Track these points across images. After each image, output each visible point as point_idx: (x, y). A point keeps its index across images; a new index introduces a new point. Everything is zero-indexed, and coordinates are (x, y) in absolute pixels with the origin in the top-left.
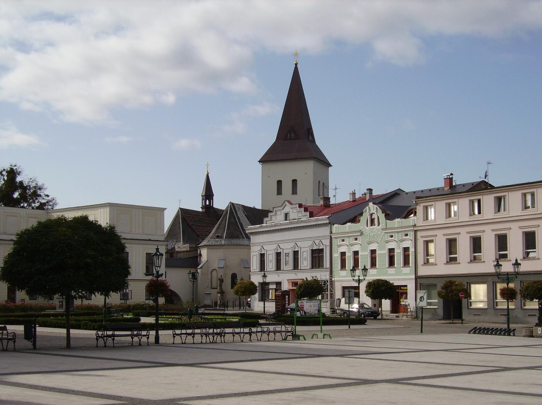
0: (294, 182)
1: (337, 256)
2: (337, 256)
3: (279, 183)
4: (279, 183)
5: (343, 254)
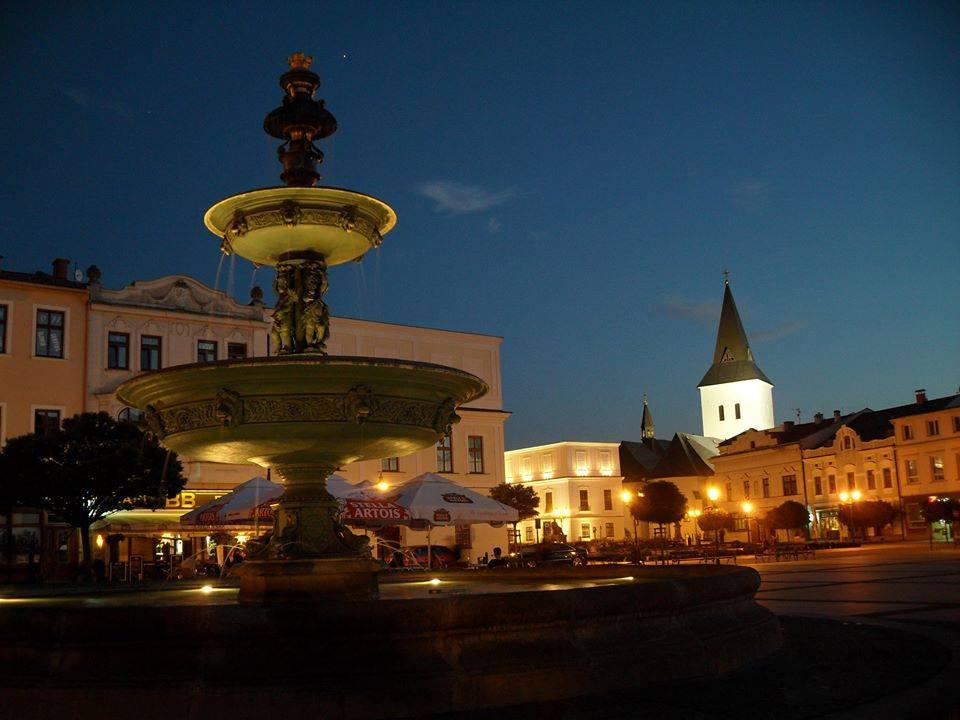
0: (737, 407)
1: (810, 481)
2: (810, 481)
3: (721, 409)
4: (721, 409)
5: (817, 480)
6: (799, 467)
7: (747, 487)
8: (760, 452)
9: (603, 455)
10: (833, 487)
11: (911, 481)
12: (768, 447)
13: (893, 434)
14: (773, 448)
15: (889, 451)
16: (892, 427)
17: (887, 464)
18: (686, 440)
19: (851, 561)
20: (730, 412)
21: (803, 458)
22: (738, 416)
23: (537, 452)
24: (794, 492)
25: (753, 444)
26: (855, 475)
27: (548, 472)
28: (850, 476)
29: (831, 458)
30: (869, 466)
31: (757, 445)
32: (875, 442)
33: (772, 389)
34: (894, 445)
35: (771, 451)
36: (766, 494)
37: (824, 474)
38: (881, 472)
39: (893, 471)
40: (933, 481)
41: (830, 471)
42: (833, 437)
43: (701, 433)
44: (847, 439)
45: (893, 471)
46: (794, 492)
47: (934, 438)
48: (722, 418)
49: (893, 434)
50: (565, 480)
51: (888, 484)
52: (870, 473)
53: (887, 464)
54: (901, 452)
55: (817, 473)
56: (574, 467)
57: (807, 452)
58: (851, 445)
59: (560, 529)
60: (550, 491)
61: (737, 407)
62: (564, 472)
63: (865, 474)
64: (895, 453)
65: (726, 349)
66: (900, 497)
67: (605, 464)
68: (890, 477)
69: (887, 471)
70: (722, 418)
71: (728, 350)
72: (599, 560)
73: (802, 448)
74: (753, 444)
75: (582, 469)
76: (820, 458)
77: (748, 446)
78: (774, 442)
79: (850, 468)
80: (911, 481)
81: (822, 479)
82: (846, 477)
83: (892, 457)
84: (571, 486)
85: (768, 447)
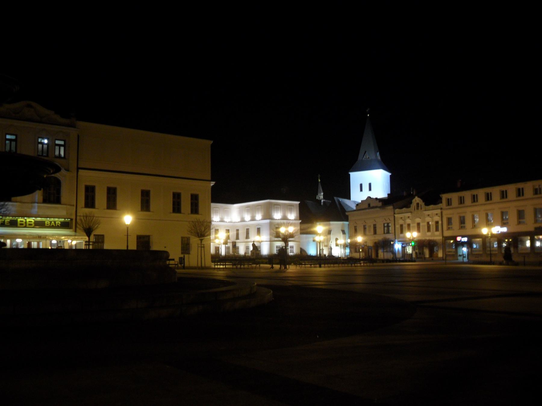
0: (370, 185)
1: (398, 226)
2: (398, 226)
4: (361, 185)
6: (392, 219)
7: (365, 228)
8: (372, 210)
9: (290, 208)
10: (402, 232)
11: (448, 229)
12: (376, 207)
13: (441, 202)
14: (380, 207)
15: (439, 211)
16: (441, 199)
17: (437, 218)
18: (339, 201)
19: (410, 267)
20: (366, 187)
21: (394, 214)
22: (370, 189)
23: (253, 205)
24: (388, 232)
25: (369, 205)
26: (421, 224)
27: (259, 216)
28: (418, 224)
29: (409, 214)
30: (428, 219)
31: (371, 205)
32: (432, 206)
33: (390, 176)
34: (441, 209)
35: (378, 209)
36: (375, 233)
37: (405, 223)
38: (434, 223)
39: (440, 222)
40: (460, 229)
41: (408, 221)
42: (411, 203)
43: (349, 197)
44: (418, 204)
45: (440, 222)
46: (388, 232)
47: (462, 205)
48: (361, 190)
49: (441, 202)
50: (268, 221)
51: (437, 230)
52: (428, 223)
53: (437, 218)
54: (445, 212)
55: (401, 222)
56: (273, 214)
57: (397, 210)
58: (420, 208)
59: (238, 248)
60: (248, 228)
61: (370, 185)
62: (268, 216)
63: (426, 224)
64: (442, 213)
65: (365, 152)
66: (443, 237)
67: (291, 213)
68: (438, 226)
69: (437, 223)
70: (361, 190)
71: (367, 153)
72: (220, 268)
73: (395, 208)
74: (369, 205)
75: (277, 215)
76: (403, 214)
77: (367, 206)
78: (380, 204)
79: (418, 220)
80: (448, 229)
81: (404, 226)
82: (416, 225)
83: (440, 215)
84: (271, 224)
85: (376, 207)
